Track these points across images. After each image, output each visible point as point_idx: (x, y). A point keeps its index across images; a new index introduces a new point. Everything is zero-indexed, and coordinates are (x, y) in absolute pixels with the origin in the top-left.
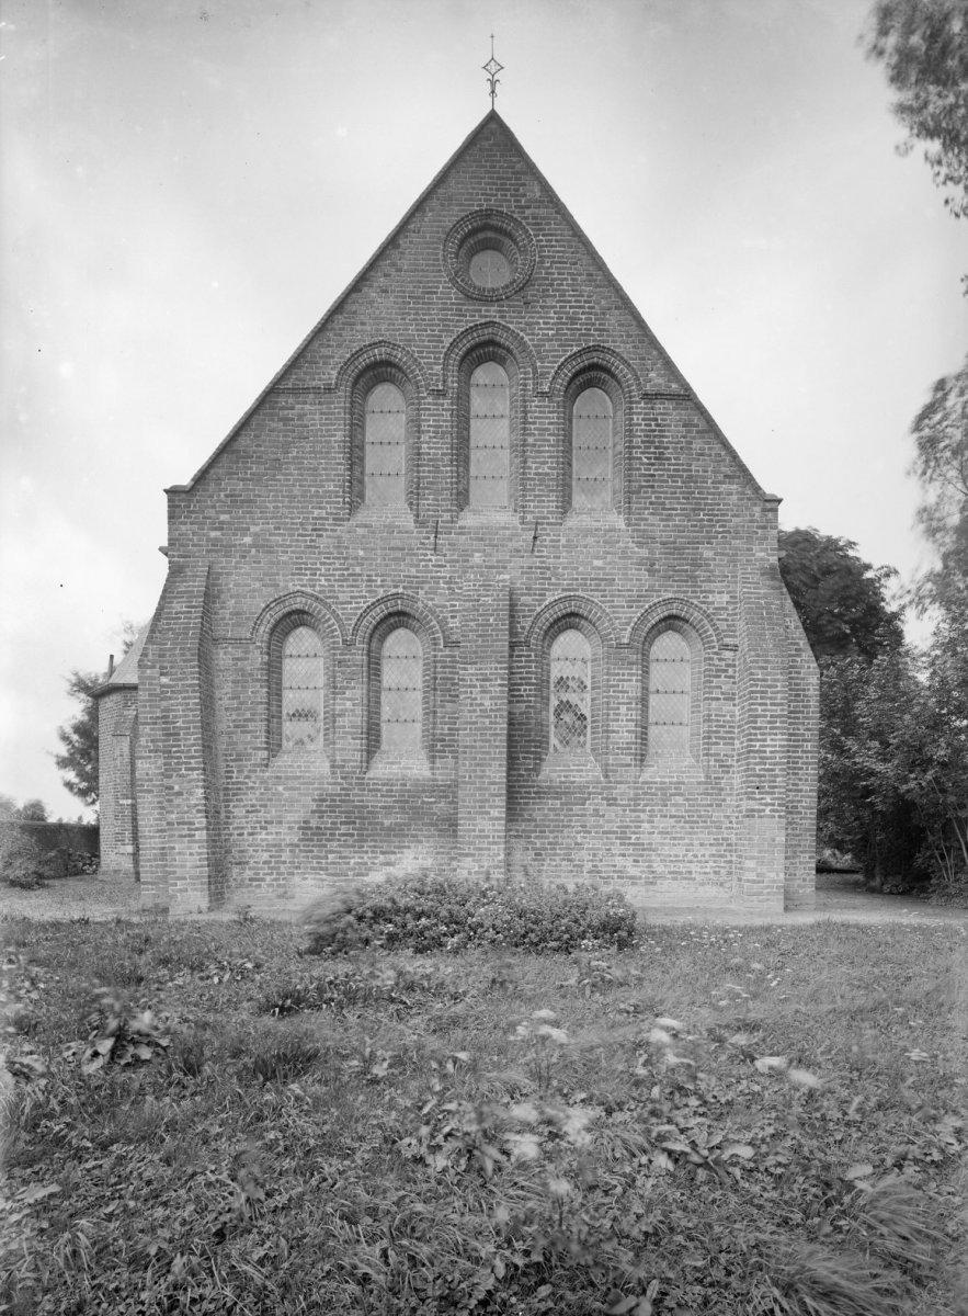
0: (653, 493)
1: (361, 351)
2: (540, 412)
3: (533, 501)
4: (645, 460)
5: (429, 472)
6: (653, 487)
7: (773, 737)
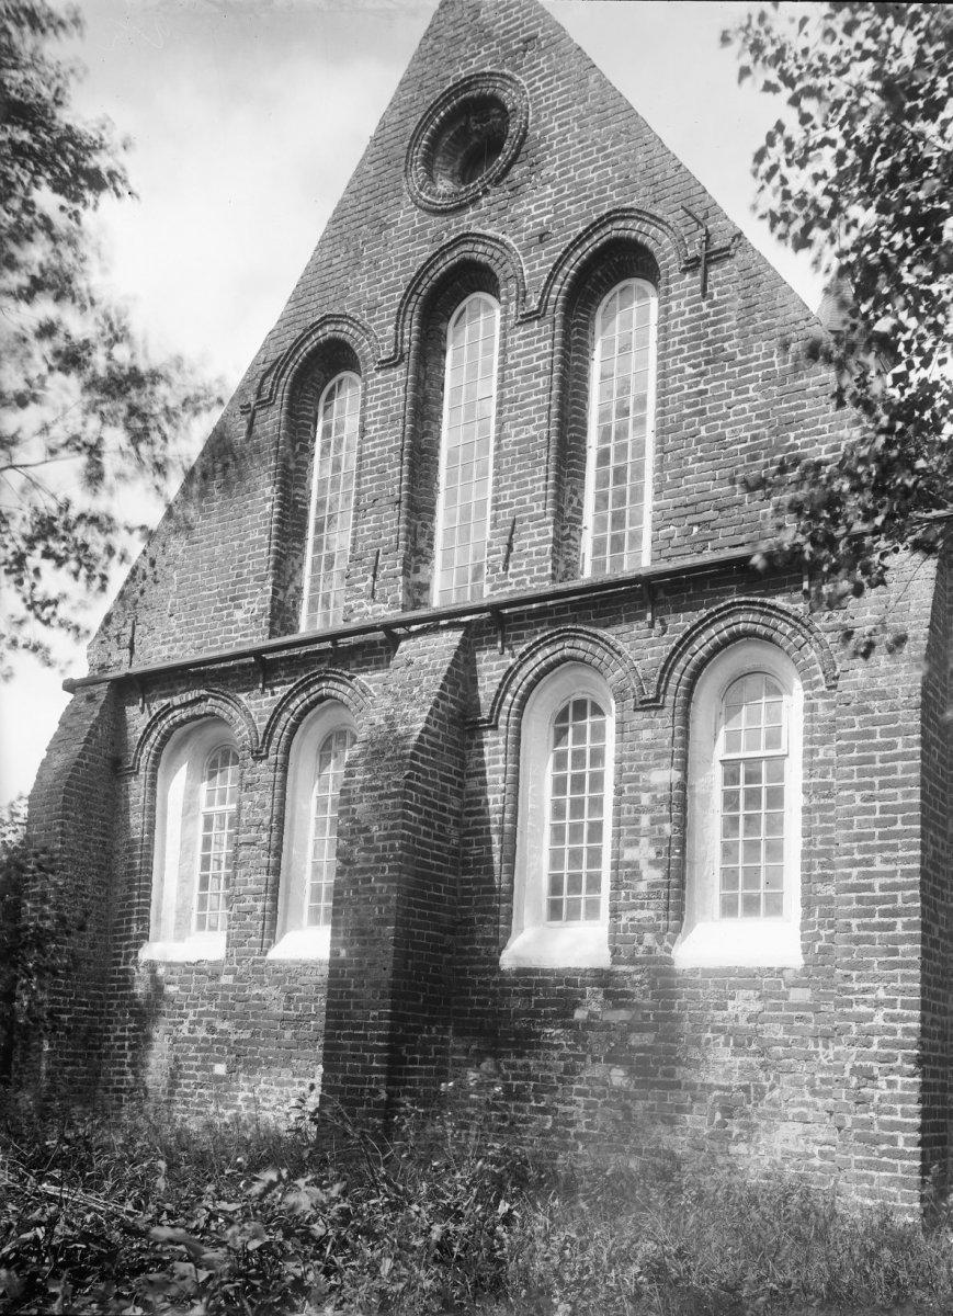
0: (702, 423)
1: (314, 328)
2: (527, 345)
3: (510, 487)
4: (690, 371)
5: (372, 481)
6: (702, 412)
7: (887, 854)
